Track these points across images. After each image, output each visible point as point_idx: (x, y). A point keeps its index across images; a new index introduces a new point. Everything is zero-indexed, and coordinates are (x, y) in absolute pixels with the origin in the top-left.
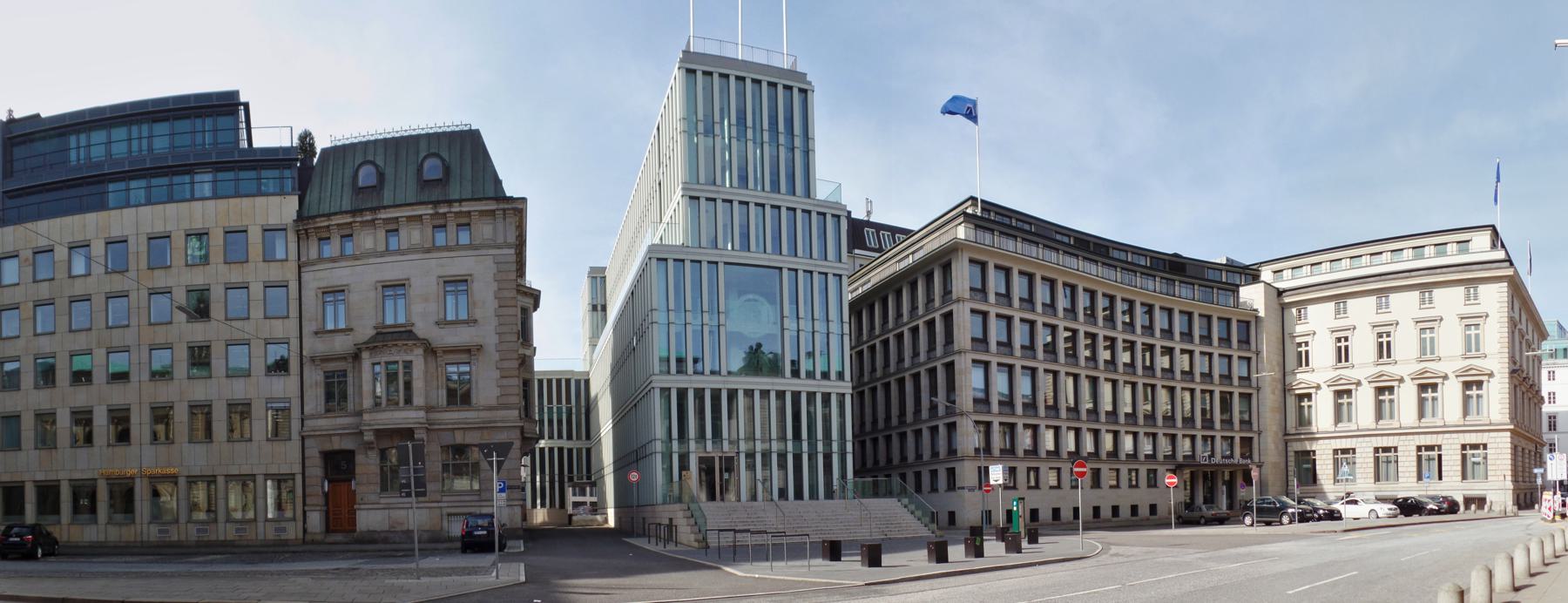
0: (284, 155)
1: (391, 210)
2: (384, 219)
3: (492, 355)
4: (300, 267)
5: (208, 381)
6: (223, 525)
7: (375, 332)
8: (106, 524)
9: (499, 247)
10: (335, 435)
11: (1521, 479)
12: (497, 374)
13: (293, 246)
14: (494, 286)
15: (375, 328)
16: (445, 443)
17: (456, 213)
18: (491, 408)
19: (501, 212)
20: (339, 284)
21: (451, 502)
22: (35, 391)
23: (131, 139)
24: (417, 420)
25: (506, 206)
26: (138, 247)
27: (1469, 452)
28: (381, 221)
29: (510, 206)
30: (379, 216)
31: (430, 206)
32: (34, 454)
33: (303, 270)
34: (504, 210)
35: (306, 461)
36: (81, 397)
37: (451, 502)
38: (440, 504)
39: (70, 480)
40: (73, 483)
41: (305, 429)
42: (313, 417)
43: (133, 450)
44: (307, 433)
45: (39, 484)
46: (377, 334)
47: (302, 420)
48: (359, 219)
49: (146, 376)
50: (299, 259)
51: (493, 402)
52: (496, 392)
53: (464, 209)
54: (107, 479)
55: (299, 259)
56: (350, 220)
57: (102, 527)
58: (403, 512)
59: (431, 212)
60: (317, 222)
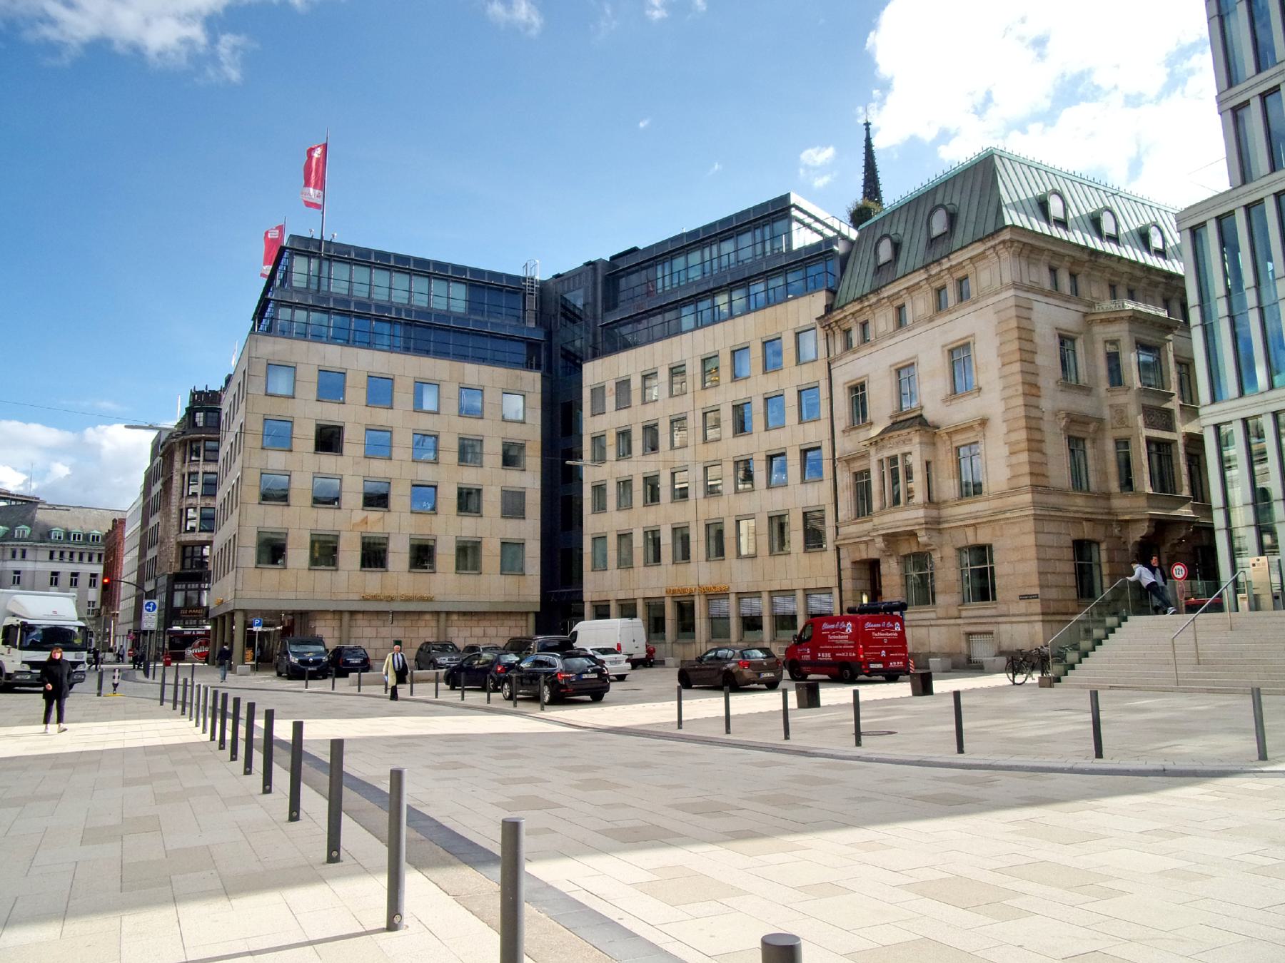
0: (806, 254)
1: (891, 286)
2: (888, 297)
3: (998, 428)
4: (829, 364)
5: (752, 493)
6: (670, 645)
7: (891, 421)
8: (673, 643)
9: (997, 293)
10: (860, 542)
11: (757, 444)
12: (1005, 450)
13: (822, 344)
14: (997, 342)
15: (891, 417)
16: (961, 544)
17: (948, 269)
18: (1000, 495)
19: (991, 251)
20: (859, 376)
21: (971, 618)
22: (617, 513)
23: (807, 277)
24: (916, 521)
25: (992, 243)
26: (694, 369)
27: (777, 600)
28: (886, 300)
29: (997, 242)
30: (882, 296)
31: (922, 271)
32: (672, 568)
33: (832, 367)
34: (994, 247)
35: (842, 572)
36: (376, 522)
37: (971, 618)
38: (959, 621)
39: (591, 602)
40: (619, 603)
41: (839, 537)
42: (848, 524)
43: (692, 566)
44: (842, 542)
45: (622, 603)
46: (893, 424)
47: (837, 527)
48: (866, 304)
49: (701, 493)
50: (828, 356)
51: (1004, 486)
52: (1007, 473)
53: (954, 263)
54: (707, 595)
55: (828, 356)
56: (859, 307)
57: (669, 646)
58: (923, 631)
59: (925, 276)
60: (834, 317)
